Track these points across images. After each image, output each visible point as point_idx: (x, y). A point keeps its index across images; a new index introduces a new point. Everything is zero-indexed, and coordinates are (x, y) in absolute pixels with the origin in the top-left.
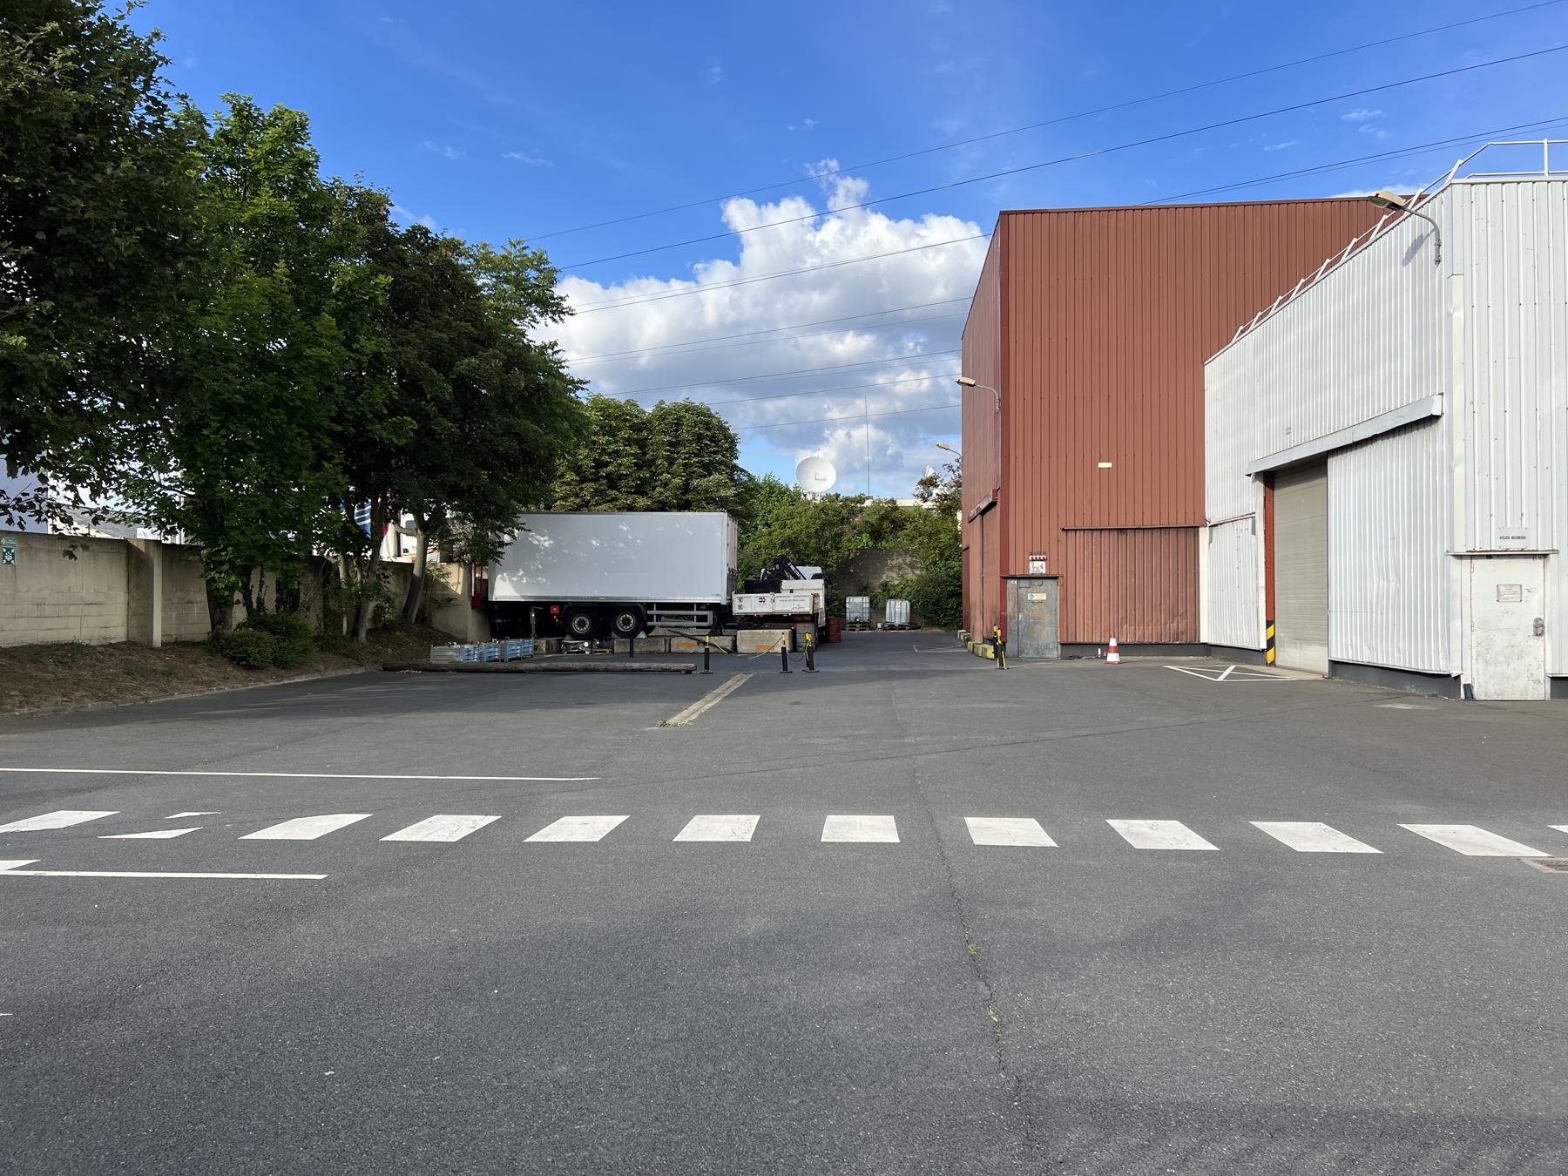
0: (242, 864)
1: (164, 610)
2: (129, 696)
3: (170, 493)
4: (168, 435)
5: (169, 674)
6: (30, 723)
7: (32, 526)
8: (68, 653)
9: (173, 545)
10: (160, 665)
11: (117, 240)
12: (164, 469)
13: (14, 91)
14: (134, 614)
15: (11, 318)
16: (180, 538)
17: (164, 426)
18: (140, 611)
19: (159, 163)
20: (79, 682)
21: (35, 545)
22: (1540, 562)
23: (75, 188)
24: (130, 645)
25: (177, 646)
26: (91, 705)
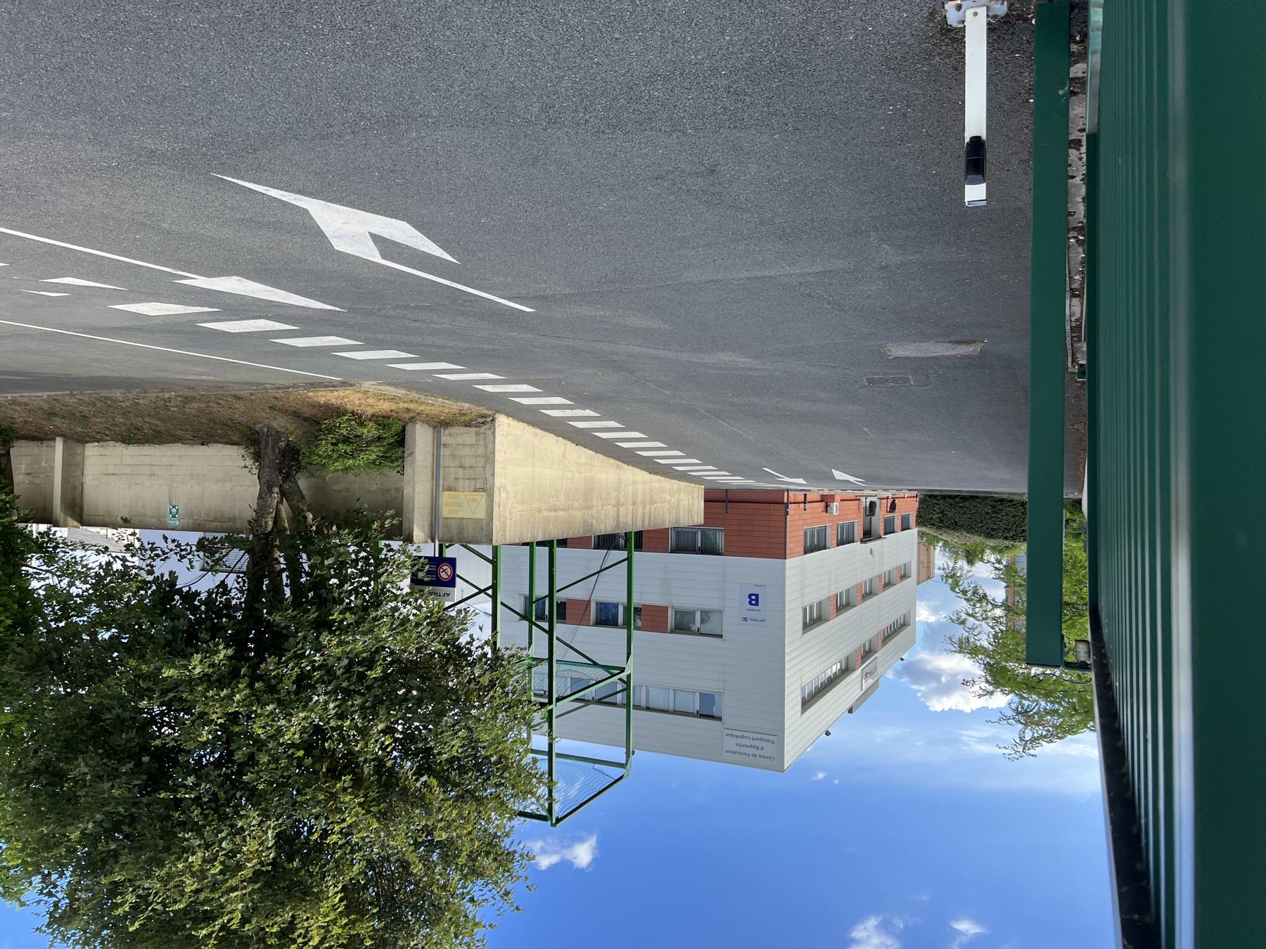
0: (9, 243)
1: (52, 468)
2: (86, 398)
3: (45, 568)
4: (44, 616)
5: (51, 414)
6: (164, 386)
7: (155, 536)
8: (132, 436)
9: (38, 522)
10: (58, 421)
11: (86, 770)
12: (49, 588)
13: (164, 866)
14: (78, 465)
15: (169, 691)
16: (37, 529)
17: (51, 620)
18: (73, 468)
19: (47, 844)
20: (125, 414)
21: (154, 521)
22: (651, 706)
23: (118, 804)
24: (83, 440)
25: (41, 437)
26: (117, 394)
